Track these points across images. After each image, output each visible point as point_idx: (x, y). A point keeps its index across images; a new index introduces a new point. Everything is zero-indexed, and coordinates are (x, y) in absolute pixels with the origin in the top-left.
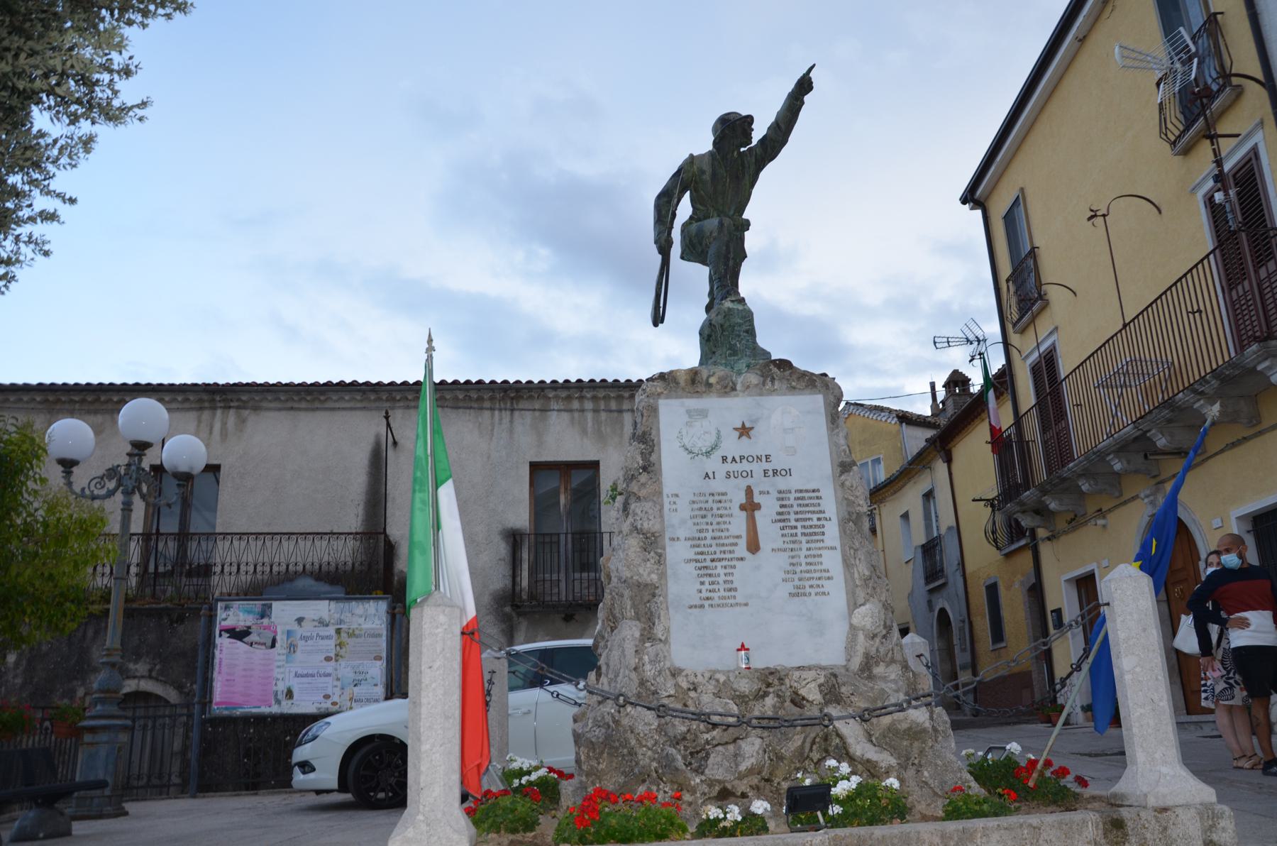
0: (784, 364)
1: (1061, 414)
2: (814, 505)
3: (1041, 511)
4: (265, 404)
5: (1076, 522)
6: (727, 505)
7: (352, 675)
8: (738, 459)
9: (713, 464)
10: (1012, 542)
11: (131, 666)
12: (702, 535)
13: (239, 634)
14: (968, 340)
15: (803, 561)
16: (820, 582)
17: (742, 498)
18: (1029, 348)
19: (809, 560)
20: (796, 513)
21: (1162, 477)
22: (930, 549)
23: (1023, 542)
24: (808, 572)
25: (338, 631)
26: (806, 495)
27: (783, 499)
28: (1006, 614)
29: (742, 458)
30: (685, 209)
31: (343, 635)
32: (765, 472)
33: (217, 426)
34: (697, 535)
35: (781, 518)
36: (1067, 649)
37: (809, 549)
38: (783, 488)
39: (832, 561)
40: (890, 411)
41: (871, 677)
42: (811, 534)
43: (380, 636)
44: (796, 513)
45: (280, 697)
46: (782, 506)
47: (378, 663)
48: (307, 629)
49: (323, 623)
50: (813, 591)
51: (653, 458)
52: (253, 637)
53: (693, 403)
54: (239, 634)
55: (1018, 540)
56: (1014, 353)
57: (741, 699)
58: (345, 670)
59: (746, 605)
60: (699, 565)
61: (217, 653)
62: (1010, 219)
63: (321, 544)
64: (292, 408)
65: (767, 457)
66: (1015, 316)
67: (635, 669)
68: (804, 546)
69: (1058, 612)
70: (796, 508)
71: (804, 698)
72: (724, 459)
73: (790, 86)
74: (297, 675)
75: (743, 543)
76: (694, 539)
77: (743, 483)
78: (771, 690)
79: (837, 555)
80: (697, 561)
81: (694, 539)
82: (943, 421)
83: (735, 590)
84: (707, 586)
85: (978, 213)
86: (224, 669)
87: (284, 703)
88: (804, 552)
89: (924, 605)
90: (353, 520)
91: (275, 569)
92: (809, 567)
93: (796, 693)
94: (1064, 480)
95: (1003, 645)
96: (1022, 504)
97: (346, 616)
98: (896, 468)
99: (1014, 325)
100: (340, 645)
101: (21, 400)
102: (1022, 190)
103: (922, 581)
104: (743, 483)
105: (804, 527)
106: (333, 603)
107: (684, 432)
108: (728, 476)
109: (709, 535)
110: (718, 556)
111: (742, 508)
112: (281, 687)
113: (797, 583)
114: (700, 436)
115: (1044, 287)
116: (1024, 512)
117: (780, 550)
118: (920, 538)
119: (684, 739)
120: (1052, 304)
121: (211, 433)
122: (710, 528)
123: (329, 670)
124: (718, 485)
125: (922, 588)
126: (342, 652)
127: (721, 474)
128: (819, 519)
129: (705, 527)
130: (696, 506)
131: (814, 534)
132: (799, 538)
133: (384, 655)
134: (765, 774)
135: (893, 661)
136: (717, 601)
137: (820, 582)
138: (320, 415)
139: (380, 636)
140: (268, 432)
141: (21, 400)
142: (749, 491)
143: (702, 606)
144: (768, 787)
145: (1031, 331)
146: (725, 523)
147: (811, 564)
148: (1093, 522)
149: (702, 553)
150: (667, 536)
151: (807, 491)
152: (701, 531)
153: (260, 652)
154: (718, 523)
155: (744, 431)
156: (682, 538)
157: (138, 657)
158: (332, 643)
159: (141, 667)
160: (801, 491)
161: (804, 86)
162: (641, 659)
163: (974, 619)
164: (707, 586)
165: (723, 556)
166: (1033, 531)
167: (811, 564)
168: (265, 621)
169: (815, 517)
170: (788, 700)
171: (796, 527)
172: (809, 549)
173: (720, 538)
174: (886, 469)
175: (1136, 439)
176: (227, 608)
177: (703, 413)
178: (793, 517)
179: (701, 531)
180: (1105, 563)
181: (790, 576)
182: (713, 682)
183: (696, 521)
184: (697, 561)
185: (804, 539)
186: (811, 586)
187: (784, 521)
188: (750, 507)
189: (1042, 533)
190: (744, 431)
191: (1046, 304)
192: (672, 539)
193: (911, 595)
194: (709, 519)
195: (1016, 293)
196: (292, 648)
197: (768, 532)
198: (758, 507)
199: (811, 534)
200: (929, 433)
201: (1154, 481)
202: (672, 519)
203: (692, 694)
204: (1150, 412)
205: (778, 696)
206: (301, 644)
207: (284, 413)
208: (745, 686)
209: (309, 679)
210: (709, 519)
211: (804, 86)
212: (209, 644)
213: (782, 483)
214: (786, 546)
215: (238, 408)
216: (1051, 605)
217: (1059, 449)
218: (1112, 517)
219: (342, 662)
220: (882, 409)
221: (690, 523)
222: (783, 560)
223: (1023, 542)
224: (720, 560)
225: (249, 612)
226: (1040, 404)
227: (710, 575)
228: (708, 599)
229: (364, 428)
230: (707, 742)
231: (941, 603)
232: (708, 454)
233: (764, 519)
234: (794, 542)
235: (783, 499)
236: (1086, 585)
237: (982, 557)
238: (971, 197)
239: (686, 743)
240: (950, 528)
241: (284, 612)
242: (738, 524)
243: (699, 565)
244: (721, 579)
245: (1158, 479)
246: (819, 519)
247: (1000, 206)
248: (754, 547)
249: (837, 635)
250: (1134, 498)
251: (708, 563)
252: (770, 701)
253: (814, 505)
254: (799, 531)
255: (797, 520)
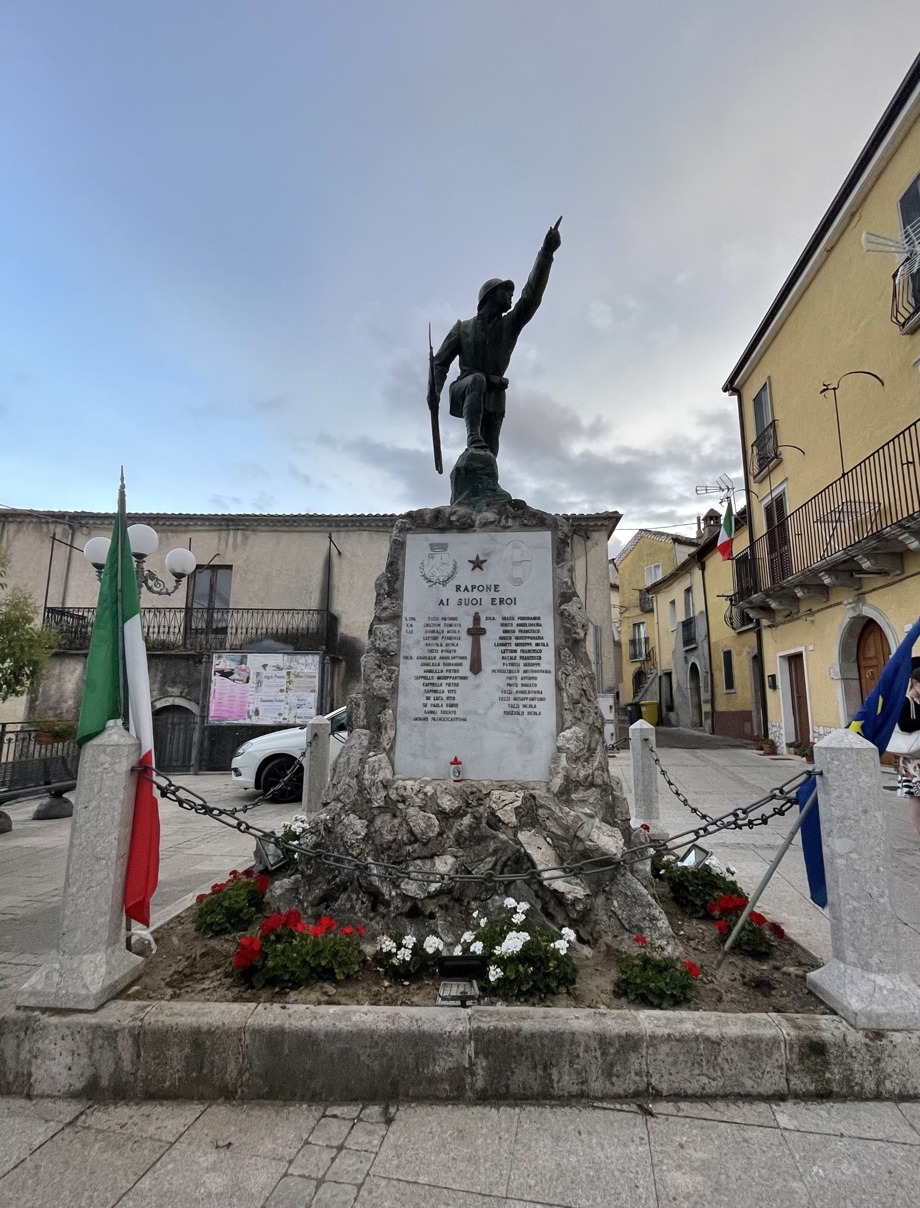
0: (520, 505)
1: (785, 541)
2: (534, 631)
3: (765, 609)
4: (259, 528)
5: (790, 617)
6: (457, 629)
7: (297, 702)
8: (470, 588)
9: (448, 592)
10: (743, 625)
11: (170, 689)
12: (433, 655)
13: (226, 674)
14: (721, 488)
15: (519, 682)
16: (533, 703)
17: (468, 623)
18: (764, 494)
19: (525, 682)
20: (517, 638)
21: (864, 590)
22: (688, 624)
23: (751, 626)
24: (523, 692)
25: (288, 673)
26: (528, 622)
27: (506, 625)
28: (736, 671)
29: (473, 587)
30: (455, 369)
31: (292, 676)
32: (493, 600)
33: (231, 541)
34: (427, 655)
35: (503, 643)
36: (779, 705)
37: (525, 672)
38: (506, 616)
39: (545, 684)
40: (668, 535)
41: (569, 802)
42: (528, 658)
43: (314, 677)
44: (517, 638)
45: (251, 713)
46: (505, 632)
47: (313, 694)
48: (269, 671)
49: (279, 668)
50: (526, 710)
51: (397, 586)
52: (235, 676)
53: (436, 538)
54: (226, 674)
55: (748, 624)
56: (753, 497)
57: (443, 815)
58: (292, 698)
59: (464, 720)
60: (426, 681)
61: (212, 685)
62: (758, 401)
63: (288, 617)
64: (276, 531)
65: (496, 587)
66: (756, 471)
67: (356, 777)
68: (522, 668)
69: (773, 677)
70: (517, 634)
71: (500, 820)
72: (458, 588)
73: (541, 244)
74: (262, 701)
75: (467, 664)
76: (424, 658)
77: (472, 610)
78: (470, 810)
79: (551, 678)
80: (425, 678)
81: (424, 658)
82: (702, 542)
83: (456, 706)
84: (432, 701)
85: (736, 397)
86: (217, 696)
87: (253, 718)
88: (521, 674)
89: (682, 660)
90: (314, 601)
91: (259, 631)
92: (524, 688)
93: (493, 813)
94: (783, 588)
95: (733, 691)
96: (750, 602)
97: (294, 664)
98: (669, 571)
99: (755, 477)
100: (290, 682)
101: (196, 524)
102: (769, 378)
103: (681, 644)
104: (472, 610)
105: (523, 651)
106: (286, 656)
107: (426, 563)
108: (460, 604)
109: (438, 655)
110: (445, 674)
111: (470, 632)
112: (252, 708)
113: (512, 702)
114: (439, 567)
115: (780, 449)
116: (751, 608)
117: (500, 671)
118: (681, 617)
119: (389, 848)
120: (784, 461)
121: (227, 545)
122: (439, 649)
123: (282, 698)
124: (448, 611)
125: (682, 649)
126: (291, 686)
127: (453, 602)
128: (537, 645)
129: (435, 648)
130: (429, 629)
131: (532, 658)
132: (518, 661)
133: (317, 689)
134: (456, 894)
135: (592, 785)
136: (439, 715)
137: (533, 703)
138: (295, 536)
139: (314, 677)
140: (262, 544)
141: (196, 524)
142: (477, 619)
143: (425, 719)
144: (457, 906)
145: (767, 481)
146: (453, 645)
147: (526, 685)
148: (804, 618)
149: (430, 671)
150: (402, 654)
151: (528, 618)
152: (431, 651)
153: (238, 687)
154: (447, 645)
155: (478, 564)
156: (415, 657)
157: (174, 683)
158: (285, 680)
159: (176, 691)
160: (523, 618)
161: (552, 241)
162: (363, 767)
163: (714, 672)
164: (432, 701)
165: (448, 674)
166: (758, 622)
167: (526, 685)
168: (243, 666)
169: (534, 642)
170: (484, 821)
171: (515, 651)
172: (525, 672)
173: (447, 658)
174: (663, 572)
175: (845, 562)
176: (219, 657)
177: (444, 547)
178: (514, 641)
179: (431, 651)
180: (811, 648)
181: (506, 695)
182: (421, 796)
183: (428, 642)
184: (425, 678)
185: (522, 662)
186: (525, 706)
187: (505, 645)
188: (476, 632)
189: (765, 622)
190: (478, 564)
191: (780, 462)
192: (406, 658)
193: (674, 652)
194: (439, 641)
195: (758, 454)
196: (259, 683)
197: (490, 653)
198: (483, 632)
199: (528, 658)
200: (693, 550)
201: (857, 593)
202: (407, 639)
203: (401, 806)
204: (860, 541)
205: (475, 817)
206: (265, 681)
207: (272, 533)
208: (447, 803)
209: (269, 703)
210: (439, 641)
211: (552, 241)
212: (208, 681)
213: (506, 611)
214: (505, 668)
215: (243, 530)
216: (767, 673)
217: (781, 565)
218: (818, 616)
219: (290, 693)
220: (662, 534)
221: (423, 643)
222: (501, 680)
223: (751, 626)
224: (446, 678)
225: (233, 660)
226: (770, 534)
227: (435, 691)
228: (432, 712)
229: (315, 546)
230: (409, 854)
231: (693, 659)
232: (444, 583)
233: (487, 644)
234: (513, 665)
235: (506, 625)
236: (795, 661)
237: (722, 633)
238: (731, 387)
239: (390, 852)
240: (701, 613)
241: (255, 661)
242: (464, 647)
243: (426, 681)
244: (444, 696)
245: (860, 591)
246: (537, 645)
247: (750, 393)
248: (476, 667)
249: (544, 750)
250: (838, 604)
251: (435, 681)
252: (467, 820)
253: (534, 631)
254: (519, 654)
255: (517, 645)
